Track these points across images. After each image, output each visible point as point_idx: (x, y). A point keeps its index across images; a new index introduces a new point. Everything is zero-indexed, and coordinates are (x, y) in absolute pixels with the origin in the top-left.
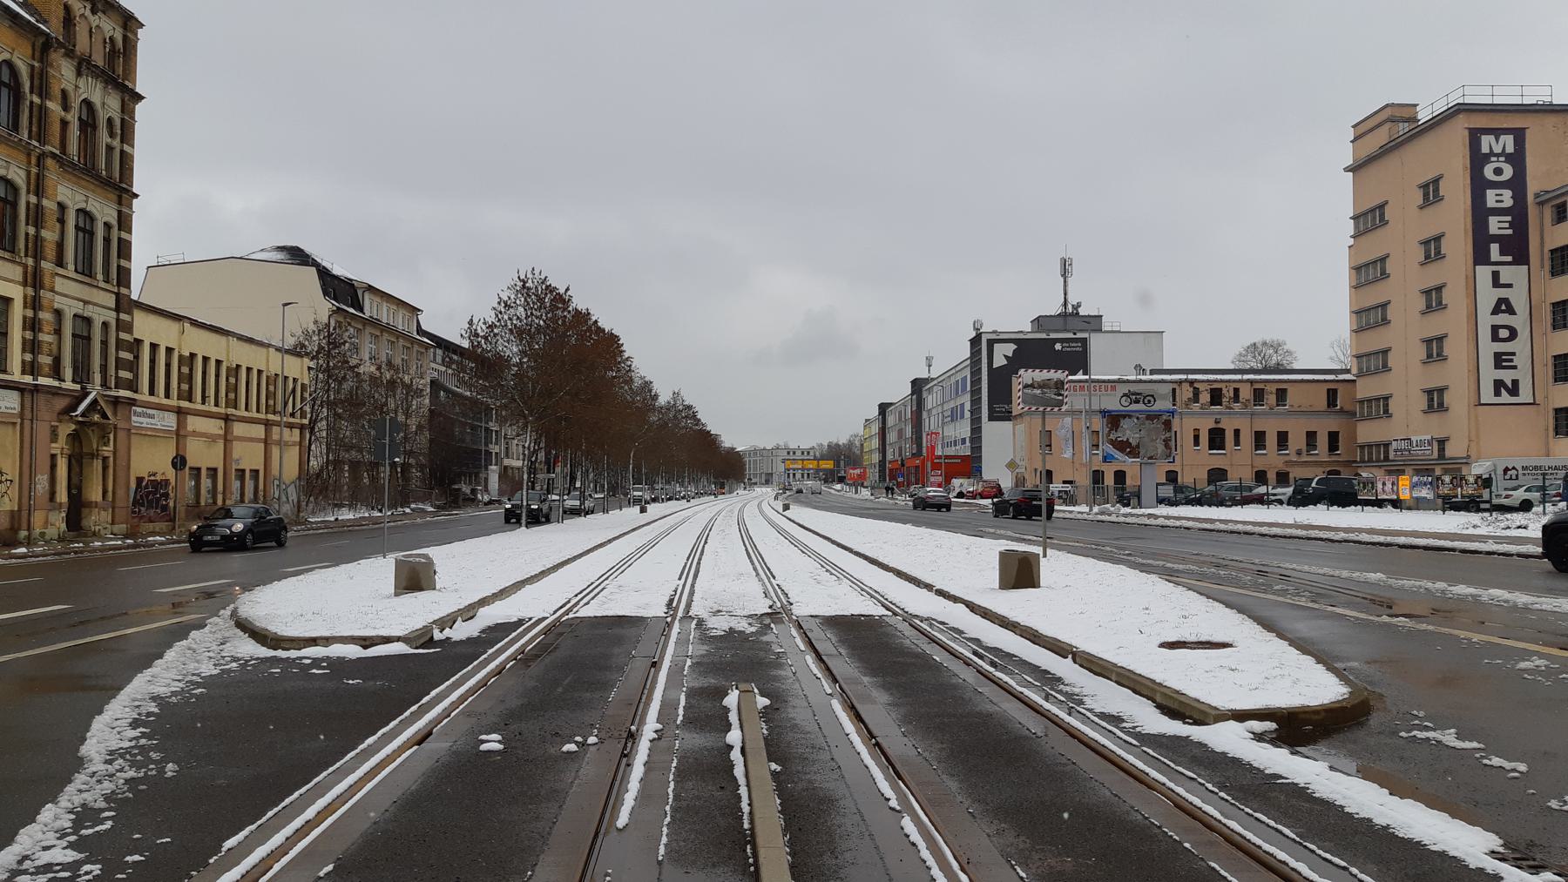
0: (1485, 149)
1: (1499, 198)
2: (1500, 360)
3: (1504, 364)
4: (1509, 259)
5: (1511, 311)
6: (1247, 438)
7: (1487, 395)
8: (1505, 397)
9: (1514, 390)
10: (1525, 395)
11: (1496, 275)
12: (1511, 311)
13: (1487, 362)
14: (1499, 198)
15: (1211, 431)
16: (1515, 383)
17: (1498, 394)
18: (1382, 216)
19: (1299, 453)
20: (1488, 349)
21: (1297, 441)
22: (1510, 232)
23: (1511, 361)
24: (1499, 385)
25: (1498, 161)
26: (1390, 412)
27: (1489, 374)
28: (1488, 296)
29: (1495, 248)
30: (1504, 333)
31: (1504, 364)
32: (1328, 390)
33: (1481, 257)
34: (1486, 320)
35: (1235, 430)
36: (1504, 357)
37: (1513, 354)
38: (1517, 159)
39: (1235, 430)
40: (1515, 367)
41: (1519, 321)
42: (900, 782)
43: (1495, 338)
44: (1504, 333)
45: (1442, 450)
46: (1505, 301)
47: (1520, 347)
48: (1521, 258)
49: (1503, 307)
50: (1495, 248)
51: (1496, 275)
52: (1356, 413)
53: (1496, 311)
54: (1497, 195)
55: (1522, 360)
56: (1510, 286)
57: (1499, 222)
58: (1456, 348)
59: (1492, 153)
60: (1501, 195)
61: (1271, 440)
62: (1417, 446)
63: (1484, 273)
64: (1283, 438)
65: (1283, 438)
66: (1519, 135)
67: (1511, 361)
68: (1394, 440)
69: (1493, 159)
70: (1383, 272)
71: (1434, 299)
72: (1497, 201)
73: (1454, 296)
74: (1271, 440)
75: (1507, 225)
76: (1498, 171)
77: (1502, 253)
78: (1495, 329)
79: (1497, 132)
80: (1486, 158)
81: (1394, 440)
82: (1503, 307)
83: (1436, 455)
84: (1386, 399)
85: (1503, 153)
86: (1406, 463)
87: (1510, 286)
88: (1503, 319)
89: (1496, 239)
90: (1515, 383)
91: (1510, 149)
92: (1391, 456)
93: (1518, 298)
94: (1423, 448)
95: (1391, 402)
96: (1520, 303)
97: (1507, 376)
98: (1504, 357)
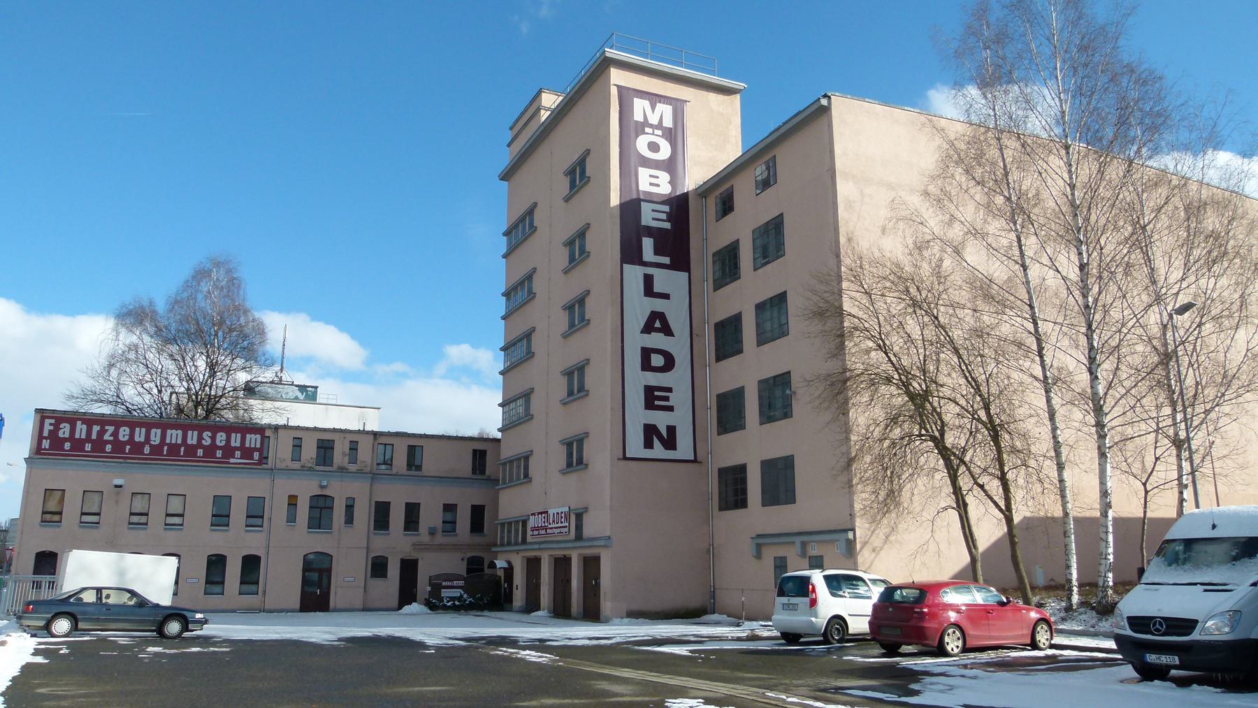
0: (638, 116)
1: (654, 181)
2: (653, 398)
3: (657, 403)
4: (666, 260)
5: (667, 330)
6: (363, 514)
7: (636, 446)
8: (658, 451)
9: (670, 442)
10: (684, 447)
11: (648, 280)
12: (667, 330)
13: (636, 398)
14: (654, 181)
15: (314, 498)
16: (671, 430)
17: (648, 444)
18: (531, 224)
19: (432, 532)
20: (638, 380)
21: (431, 517)
22: (667, 225)
23: (667, 399)
24: (650, 432)
25: (653, 134)
26: (530, 476)
27: (638, 416)
28: (639, 308)
29: (648, 244)
30: (657, 360)
31: (657, 403)
32: (475, 451)
33: (631, 254)
34: (636, 340)
35: (290, 497)
36: (656, 393)
37: (669, 390)
38: (674, 135)
39: (290, 497)
40: (671, 409)
41: (678, 345)
42: (548, 643)
43: (646, 366)
44: (657, 360)
45: (579, 527)
46: (661, 316)
47: (678, 379)
48: (681, 262)
49: (658, 324)
50: (648, 244)
51: (648, 280)
52: (499, 480)
53: (648, 328)
54: (651, 176)
55: (680, 398)
56: (666, 296)
57: (653, 211)
58: (600, 379)
59: (646, 123)
60: (657, 177)
61: (397, 517)
62: (554, 521)
63: (634, 274)
64: (412, 513)
65: (412, 513)
66: (678, 106)
67: (667, 399)
68: (532, 515)
69: (648, 130)
70: (530, 291)
71: (576, 309)
72: (651, 184)
73: (600, 309)
74: (397, 517)
75: (664, 216)
76: (654, 147)
77: (657, 252)
78: (646, 353)
79: (654, 98)
80: (641, 128)
81: (532, 515)
82: (658, 324)
83: (169, 432)
84: (527, 458)
85: (659, 126)
86: (542, 546)
87: (666, 296)
88: (656, 340)
89: (650, 231)
90: (671, 430)
91: (668, 123)
92: (529, 539)
93: (676, 314)
94: (560, 525)
95: (532, 462)
96: (678, 321)
97: (661, 420)
98: (656, 393)
